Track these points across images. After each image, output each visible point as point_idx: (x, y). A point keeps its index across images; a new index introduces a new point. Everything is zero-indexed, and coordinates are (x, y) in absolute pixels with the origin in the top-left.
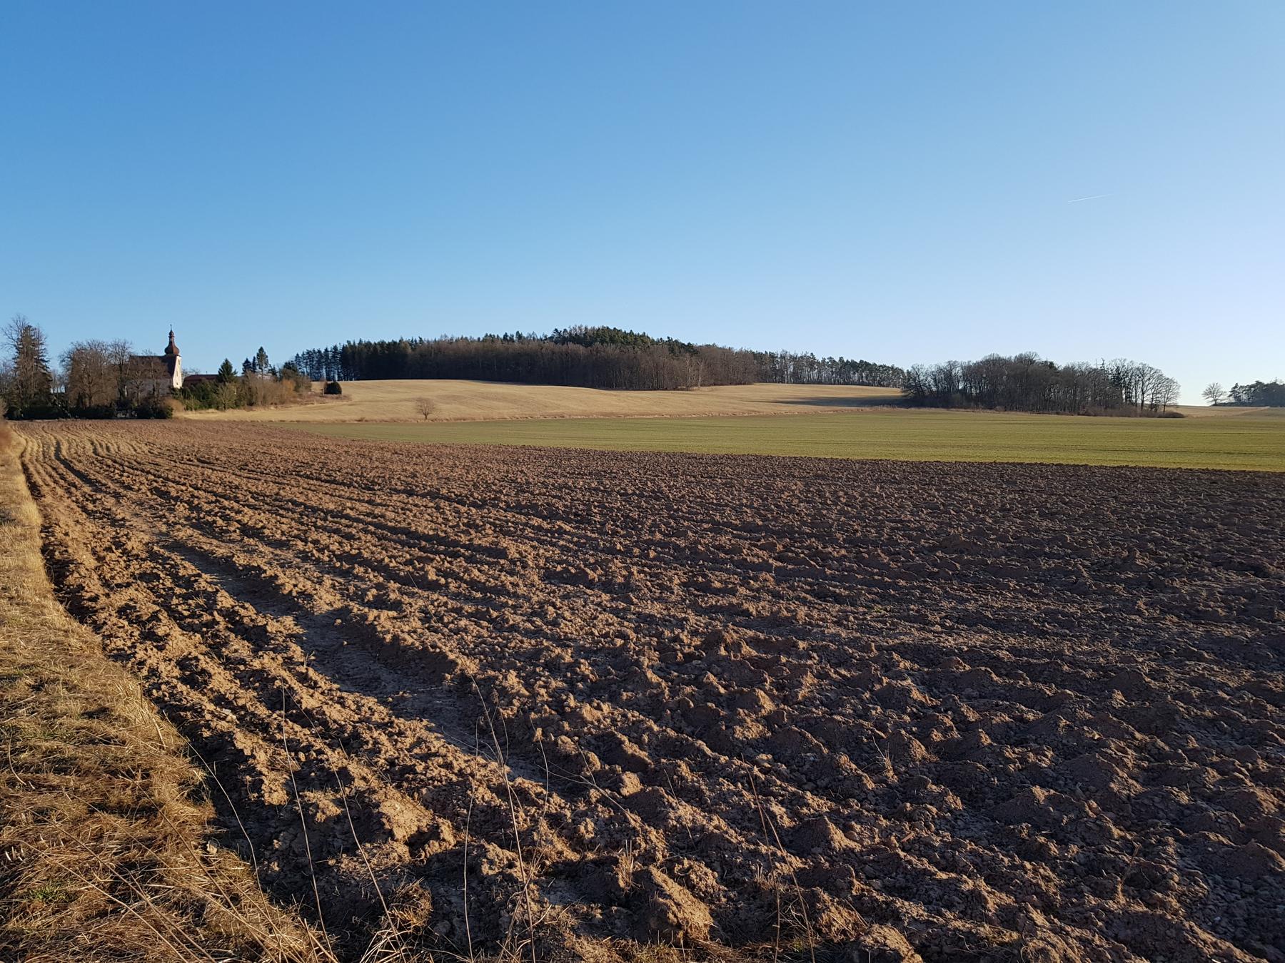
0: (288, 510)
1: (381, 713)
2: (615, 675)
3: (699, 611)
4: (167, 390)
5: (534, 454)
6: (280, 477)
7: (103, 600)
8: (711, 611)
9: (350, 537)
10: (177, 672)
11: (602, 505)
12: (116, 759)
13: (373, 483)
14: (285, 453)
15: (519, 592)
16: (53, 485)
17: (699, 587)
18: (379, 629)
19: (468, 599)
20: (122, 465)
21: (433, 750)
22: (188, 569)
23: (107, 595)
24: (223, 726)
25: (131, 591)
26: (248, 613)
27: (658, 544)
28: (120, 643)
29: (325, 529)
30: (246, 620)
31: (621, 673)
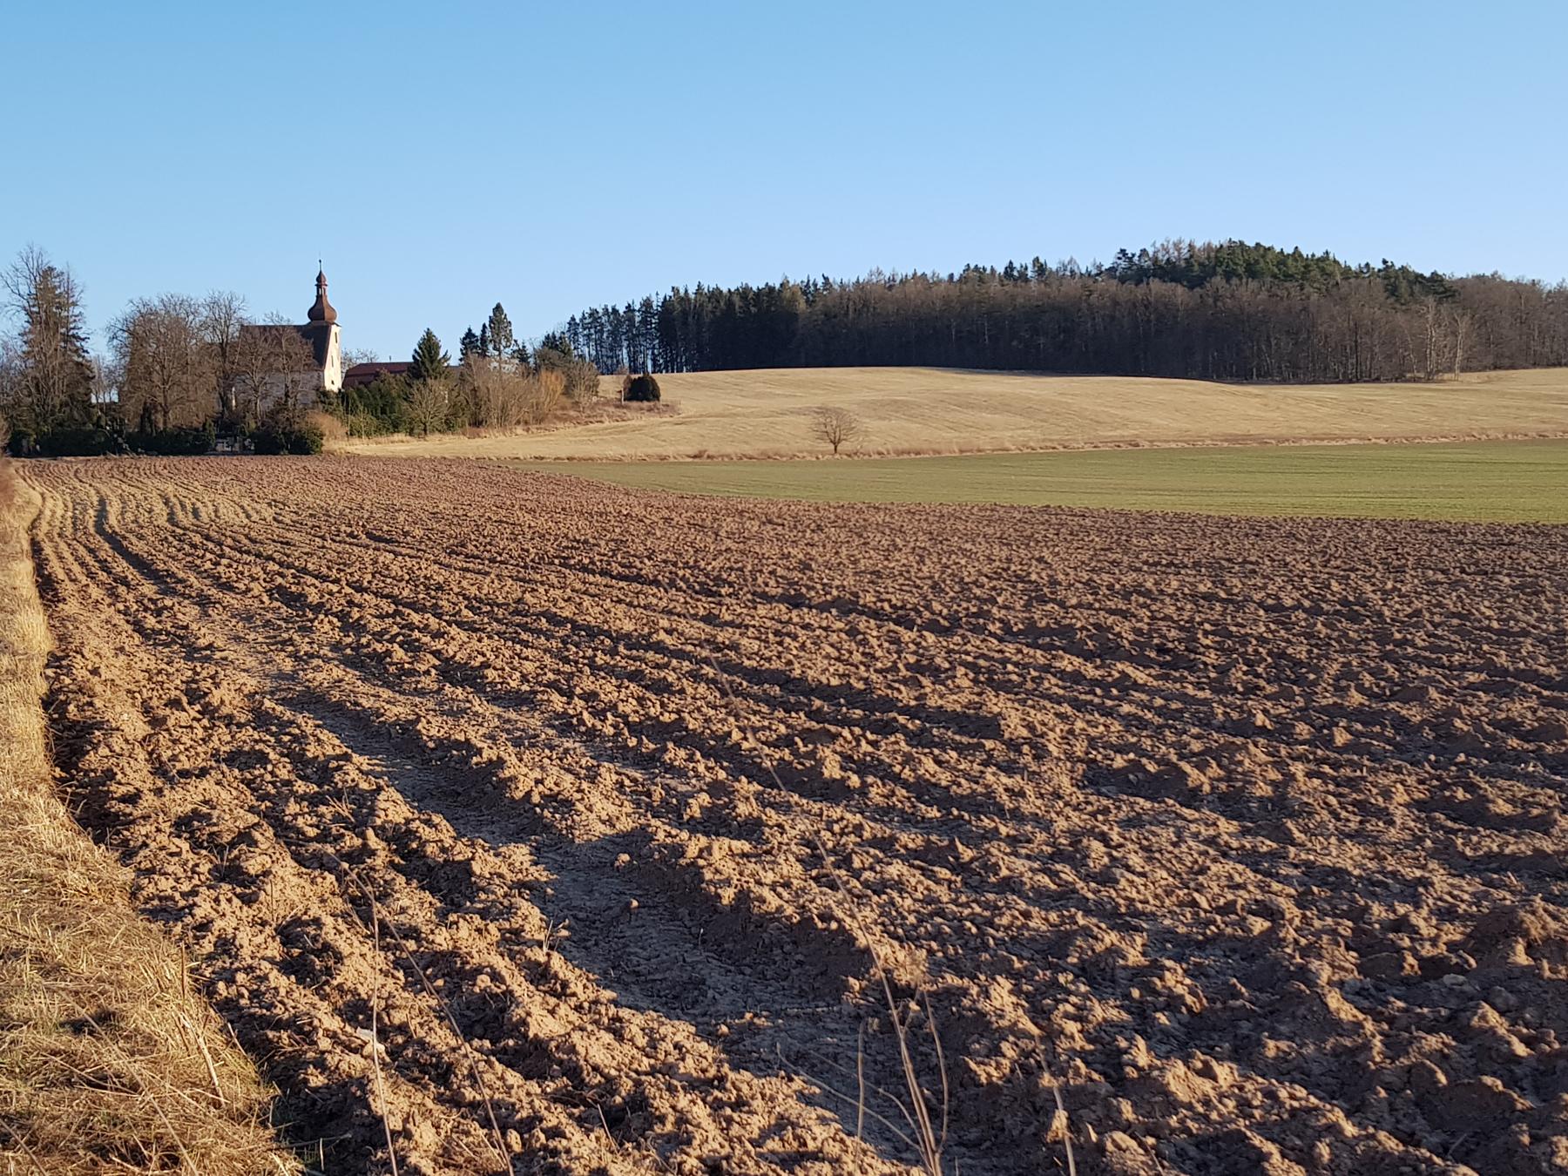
0: (539, 632)
1: (701, 1056)
2: (1249, 998)
3: (1458, 865)
4: (313, 396)
5: (1067, 525)
6: (527, 569)
7: (148, 800)
8: (1488, 866)
9: (662, 688)
10: (275, 949)
11: (1220, 630)
12: (115, 1121)
13: (719, 581)
14: (542, 523)
15: (1026, 808)
16: (84, 580)
17: (1457, 812)
18: (708, 876)
19: (910, 821)
20: (220, 544)
21: (811, 1146)
22: (326, 744)
23: (159, 792)
24: (352, 1064)
25: (207, 784)
26: (438, 836)
27: (1357, 714)
28: (165, 885)
29: (611, 671)
30: (430, 849)
31: (1264, 997)
